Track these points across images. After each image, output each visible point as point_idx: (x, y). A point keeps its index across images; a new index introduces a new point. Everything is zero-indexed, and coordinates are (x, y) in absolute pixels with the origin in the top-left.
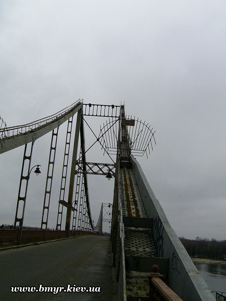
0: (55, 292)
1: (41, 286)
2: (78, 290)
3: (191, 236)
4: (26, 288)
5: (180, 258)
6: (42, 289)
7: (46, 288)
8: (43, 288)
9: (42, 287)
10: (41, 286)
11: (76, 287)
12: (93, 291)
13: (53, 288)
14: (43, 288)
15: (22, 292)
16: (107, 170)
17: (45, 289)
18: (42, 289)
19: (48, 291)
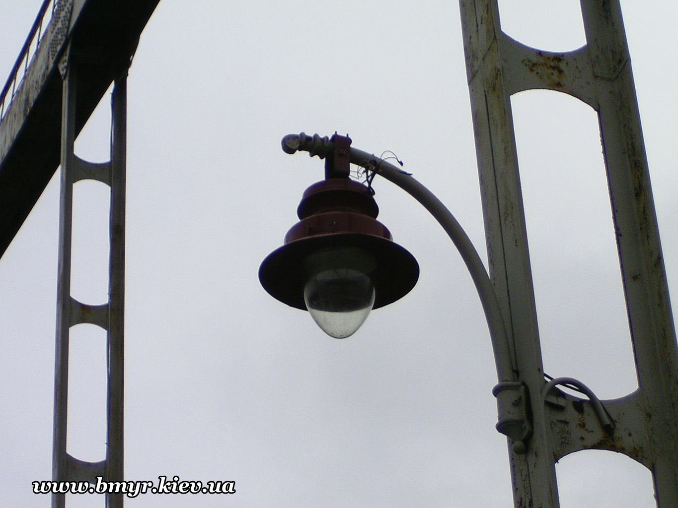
0: (133, 494)
1: (100, 479)
2: (183, 489)
3: (306, 312)
4: (67, 484)
5: (60, 199)
6: (102, 486)
7: (112, 485)
8: (105, 485)
9: (102, 482)
10: (100, 479)
11: (179, 482)
12: (112, 485)
13: (107, 483)
14: (105, 485)
15: (59, 493)
16: (293, 144)
17: (109, 486)
18: (102, 486)
19: (117, 490)
